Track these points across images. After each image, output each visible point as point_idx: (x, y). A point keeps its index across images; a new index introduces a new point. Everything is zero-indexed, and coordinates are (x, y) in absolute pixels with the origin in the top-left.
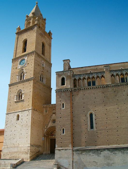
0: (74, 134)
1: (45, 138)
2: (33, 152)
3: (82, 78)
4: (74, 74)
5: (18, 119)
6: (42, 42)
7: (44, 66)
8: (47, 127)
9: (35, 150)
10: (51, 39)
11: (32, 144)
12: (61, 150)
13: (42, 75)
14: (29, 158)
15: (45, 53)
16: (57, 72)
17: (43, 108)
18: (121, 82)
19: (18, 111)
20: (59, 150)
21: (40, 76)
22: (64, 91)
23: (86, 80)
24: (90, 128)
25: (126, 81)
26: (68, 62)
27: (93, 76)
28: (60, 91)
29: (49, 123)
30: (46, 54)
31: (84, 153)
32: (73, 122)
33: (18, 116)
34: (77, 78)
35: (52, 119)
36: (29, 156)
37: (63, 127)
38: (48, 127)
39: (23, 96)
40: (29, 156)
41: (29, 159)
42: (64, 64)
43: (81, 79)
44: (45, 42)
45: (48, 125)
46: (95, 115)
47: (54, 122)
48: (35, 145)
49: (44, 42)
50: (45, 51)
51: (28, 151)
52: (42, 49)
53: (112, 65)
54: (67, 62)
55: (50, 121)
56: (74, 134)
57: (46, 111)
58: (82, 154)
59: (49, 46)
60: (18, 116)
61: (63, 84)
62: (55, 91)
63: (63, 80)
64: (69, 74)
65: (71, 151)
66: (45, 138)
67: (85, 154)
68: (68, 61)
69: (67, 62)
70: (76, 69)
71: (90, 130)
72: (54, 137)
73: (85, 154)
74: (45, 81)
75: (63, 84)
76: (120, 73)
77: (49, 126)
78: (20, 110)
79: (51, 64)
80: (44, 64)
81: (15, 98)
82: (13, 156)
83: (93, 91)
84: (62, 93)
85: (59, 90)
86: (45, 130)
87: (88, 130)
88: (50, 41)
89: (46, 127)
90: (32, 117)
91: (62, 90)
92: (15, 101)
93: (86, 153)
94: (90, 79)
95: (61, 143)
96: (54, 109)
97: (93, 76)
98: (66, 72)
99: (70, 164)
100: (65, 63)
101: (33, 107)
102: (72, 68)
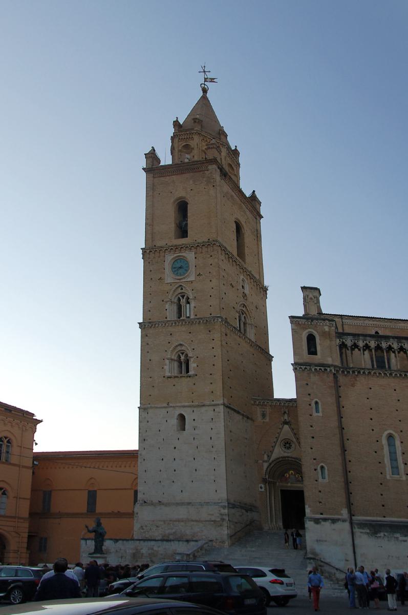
0: (351, 483)
1: (265, 487)
2: (236, 523)
3: (361, 344)
4: (345, 331)
5: (183, 427)
6: (235, 220)
7: (247, 291)
8: (268, 456)
9: (241, 516)
10: (258, 217)
11: (232, 501)
12: (321, 520)
13: (243, 314)
14: (225, 537)
15: (246, 256)
16: (292, 317)
17: (252, 404)
18: (375, 366)
19: (180, 404)
20: (317, 521)
21: (239, 317)
22: (316, 369)
23: (359, 350)
24: (391, 474)
25: (387, 367)
26: (314, 294)
27: (390, 345)
28: (305, 368)
29: (273, 447)
30: (248, 259)
31: (382, 534)
32: (346, 452)
33: (182, 418)
34: (349, 342)
35: (282, 437)
36: (226, 532)
37: (322, 462)
38: (271, 459)
39: (192, 365)
40: (225, 532)
41: (227, 543)
42: (304, 299)
43: (346, 345)
44: (242, 221)
45: (272, 452)
46: (402, 442)
47: (287, 445)
48: (240, 503)
49: (239, 221)
50: (246, 248)
51: (223, 520)
52: (237, 240)
53: (400, 323)
54: (311, 294)
55: (275, 443)
56: (351, 483)
57: (264, 415)
58: (377, 536)
59: (255, 238)
60: (182, 418)
61: (312, 350)
62: (292, 367)
63: (311, 339)
64: (326, 329)
65: (347, 525)
66: (265, 485)
67: (384, 535)
68: (316, 294)
69: (311, 294)
70: (377, 321)
71: (390, 477)
72: (289, 484)
73: (384, 535)
74: (251, 334)
75: (312, 350)
76: (373, 344)
77: (274, 456)
78: (186, 404)
79: (265, 290)
80: (247, 287)
81: (167, 367)
82: (174, 531)
83: (384, 381)
84: (312, 375)
85: (303, 365)
86: (266, 465)
87: (386, 476)
88: (258, 224)
89: (266, 458)
90: (226, 426)
91: (310, 366)
92: (168, 374)
93: (386, 534)
94: (383, 351)
95: (320, 502)
96: (285, 412)
97: (388, 344)
98: (320, 321)
99: (347, 560)
100: (308, 296)
101: (225, 399)
102: (324, 314)
